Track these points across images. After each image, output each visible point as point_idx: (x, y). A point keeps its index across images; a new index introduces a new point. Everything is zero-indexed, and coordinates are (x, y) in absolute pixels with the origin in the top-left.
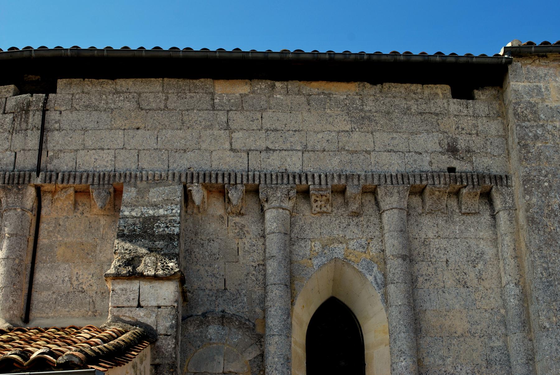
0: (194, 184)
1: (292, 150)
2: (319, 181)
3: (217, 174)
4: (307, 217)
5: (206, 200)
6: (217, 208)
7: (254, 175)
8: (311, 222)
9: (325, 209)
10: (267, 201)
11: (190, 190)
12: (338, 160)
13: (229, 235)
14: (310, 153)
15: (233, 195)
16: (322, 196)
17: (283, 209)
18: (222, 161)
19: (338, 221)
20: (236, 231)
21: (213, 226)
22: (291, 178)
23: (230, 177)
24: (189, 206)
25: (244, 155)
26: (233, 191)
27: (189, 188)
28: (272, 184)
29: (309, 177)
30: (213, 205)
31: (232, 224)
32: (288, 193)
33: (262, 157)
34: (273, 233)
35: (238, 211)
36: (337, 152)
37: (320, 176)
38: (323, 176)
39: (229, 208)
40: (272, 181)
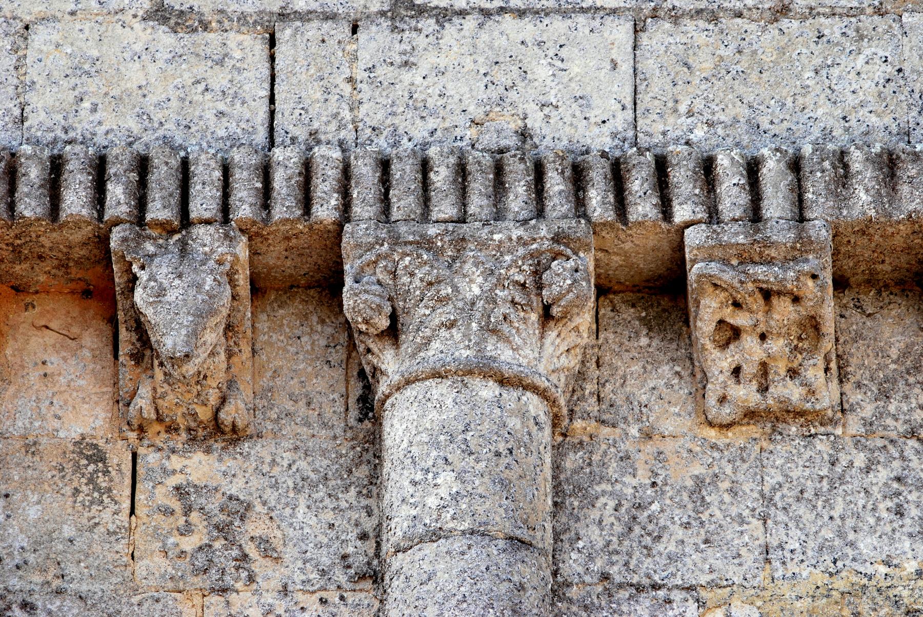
1: (566, 14)
2: (744, 199)
3: (56, 166)
4: (669, 446)
7: (307, 169)
8: (699, 482)
9: (793, 392)
10: (393, 333)
12: (880, 71)
13: (141, 568)
14: (689, 25)
15: (161, 292)
16: (767, 295)
17: (503, 381)
18: (92, 85)
19: (883, 475)
20: (189, 543)
21: (33, 513)
22: (556, 184)
25: (248, 47)
26: (163, 269)
28: (425, 217)
29: (682, 178)
30: (34, 376)
31: (163, 496)
32: (537, 274)
33: (365, 58)
34: (435, 535)
35: (204, 414)
36: (867, 22)
37: (753, 168)
38: (773, 170)
39: (145, 391)
40: (426, 201)
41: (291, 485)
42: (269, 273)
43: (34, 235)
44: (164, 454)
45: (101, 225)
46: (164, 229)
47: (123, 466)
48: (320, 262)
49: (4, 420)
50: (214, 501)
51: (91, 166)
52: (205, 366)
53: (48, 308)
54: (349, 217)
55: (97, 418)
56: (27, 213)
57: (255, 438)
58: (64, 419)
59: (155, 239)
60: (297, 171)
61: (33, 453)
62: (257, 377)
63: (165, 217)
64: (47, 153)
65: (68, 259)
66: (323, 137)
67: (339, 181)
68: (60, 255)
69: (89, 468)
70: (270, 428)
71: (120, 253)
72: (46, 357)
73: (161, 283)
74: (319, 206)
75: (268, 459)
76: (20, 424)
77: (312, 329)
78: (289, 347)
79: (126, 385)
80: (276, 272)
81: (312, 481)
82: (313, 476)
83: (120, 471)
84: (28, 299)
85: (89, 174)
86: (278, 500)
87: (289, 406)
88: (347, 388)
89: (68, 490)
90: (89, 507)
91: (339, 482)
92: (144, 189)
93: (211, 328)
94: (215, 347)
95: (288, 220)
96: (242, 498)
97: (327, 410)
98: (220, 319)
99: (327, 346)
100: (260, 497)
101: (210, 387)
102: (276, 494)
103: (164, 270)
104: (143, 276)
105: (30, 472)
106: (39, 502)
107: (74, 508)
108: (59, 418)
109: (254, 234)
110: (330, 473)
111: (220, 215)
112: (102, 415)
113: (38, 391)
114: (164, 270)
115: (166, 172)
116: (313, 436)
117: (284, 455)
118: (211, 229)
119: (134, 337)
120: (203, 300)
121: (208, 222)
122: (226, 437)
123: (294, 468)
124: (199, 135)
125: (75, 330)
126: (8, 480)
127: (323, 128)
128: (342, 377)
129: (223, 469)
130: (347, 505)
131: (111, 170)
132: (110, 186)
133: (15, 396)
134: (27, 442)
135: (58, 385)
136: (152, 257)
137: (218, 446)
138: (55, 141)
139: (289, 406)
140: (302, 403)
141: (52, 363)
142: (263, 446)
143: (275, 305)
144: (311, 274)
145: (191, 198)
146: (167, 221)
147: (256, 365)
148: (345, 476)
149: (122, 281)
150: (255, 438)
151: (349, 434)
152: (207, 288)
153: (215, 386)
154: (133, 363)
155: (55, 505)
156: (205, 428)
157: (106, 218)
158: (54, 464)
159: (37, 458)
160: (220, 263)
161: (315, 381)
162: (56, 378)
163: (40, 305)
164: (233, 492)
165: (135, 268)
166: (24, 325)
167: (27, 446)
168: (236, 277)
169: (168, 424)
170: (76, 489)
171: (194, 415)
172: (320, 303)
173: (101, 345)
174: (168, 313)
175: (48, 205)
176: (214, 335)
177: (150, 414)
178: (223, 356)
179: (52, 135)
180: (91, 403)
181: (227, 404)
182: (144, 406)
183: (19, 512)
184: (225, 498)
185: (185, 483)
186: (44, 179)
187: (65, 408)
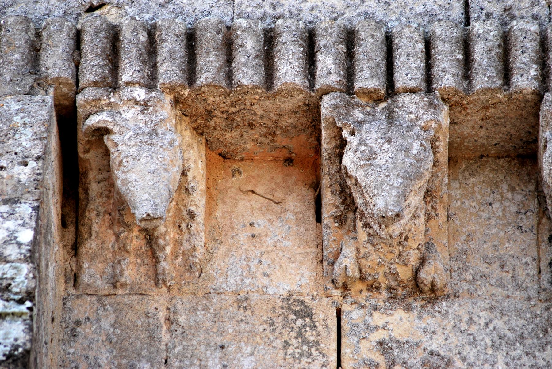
0: (126, 93)
3: (269, 39)
5: (198, 202)
6: (265, 249)
7: (506, 43)
11: (102, 132)
15: (372, 156)
23: (350, 55)
24: (91, 246)
26: (372, 134)
27: (94, 120)
30: (243, 237)
35: (405, 274)
39: (349, 251)
41: (489, 343)
42: (462, 142)
43: (248, 103)
44: (367, 311)
45: (312, 94)
46: (371, 98)
47: (329, 322)
48: (513, 132)
49: (217, 277)
50: (415, 356)
51: (302, 38)
52: (407, 228)
53: (253, 174)
54: (547, 87)
55: (302, 276)
56: (245, 82)
57: (452, 298)
58: (272, 277)
59: (363, 107)
60: (497, 43)
61: (245, 308)
62: (451, 241)
63: (373, 86)
64: (260, 26)
65: (277, 127)
66: (517, 13)
67: (537, 53)
68: (269, 123)
69: (297, 323)
70: (466, 288)
71: (331, 120)
72: (253, 220)
73: (371, 147)
74: (518, 76)
75: (466, 318)
76: (232, 281)
77: (502, 197)
78: (481, 213)
79: (330, 246)
80: (469, 142)
81: (509, 339)
82: (509, 334)
83: (326, 326)
84: (235, 166)
85: (301, 45)
86: (477, 357)
87: (483, 268)
88: (539, 254)
89: (279, 343)
90: (299, 359)
91: (535, 341)
92: (351, 60)
95: (489, 89)
96: (442, 354)
97: (521, 272)
98: (422, 184)
99: (518, 213)
100: (460, 353)
102: (475, 350)
103: (374, 135)
104: (353, 141)
105: (243, 325)
106: (252, 354)
107: (285, 359)
108: (268, 276)
109: (454, 103)
110: (526, 332)
111: (423, 86)
112: (308, 274)
113: (247, 250)
115: (372, 44)
116: (508, 297)
117: (481, 314)
118: (416, 98)
120: (411, 164)
121: (413, 91)
122: (425, 296)
123: (491, 327)
124: (398, 11)
125: (279, 195)
126: (222, 332)
127: (517, 4)
128: (534, 242)
129: (423, 326)
130: (545, 363)
131: (321, 42)
132: (320, 57)
133: (226, 255)
134: (239, 297)
135: (265, 246)
136: (361, 123)
137: (417, 304)
138: (263, 17)
139: (483, 268)
140: (496, 266)
141: (259, 225)
142: (460, 305)
143: (466, 173)
144: (502, 144)
145: (396, 69)
146: (375, 90)
147: (451, 229)
148: (541, 336)
149: (330, 146)
150: (452, 298)
151: (543, 296)
152: (415, 152)
153: (415, 247)
154: (337, 225)
155: (267, 356)
156: (404, 287)
157: (317, 86)
158: (265, 318)
159: (249, 313)
160: (425, 129)
161: (507, 245)
162: (263, 239)
163: (246, 171)
164: (434, 347)
165: (345, 134)
166: (232, 190)
167: (239, 301)
168: (437, 143)
169: (370, 283)
170: (286, 342)
171: (395, 275)
172: (510, 172)
173: (304, 209)
174: (379, 175)
175: (264, 74)
176: (417, 198)
177: (354, 272)
178: (422, 220)
179: (262, 10)
180: (297, 262)
181: (427, 264)
182: (348, 265)
183: (235, 362)
184: (426, 354)
185: (387, 338)
186: (259, 50)
187: (273, 266)
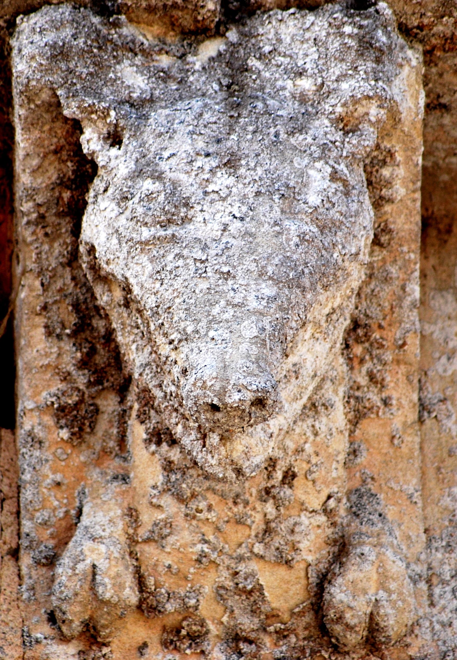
15: (176, 211)
39: (103, 518)
46: (172, 24)
52: (291, 445)
59: (147, 54)
62: (432, 484)
71: (45, 96)
73: (175, 184)
93: (317, 325)
94: (319, 388)
98: (337, 300)
101: (302, 507)
104: (117, 163)
114: (183, 145)
119: (70, 355)
120: (302, 237)
136: (141, 106)
147: (430, 448)
149: (41, 181)
154: (65, 434)
165: (91, 140)
168: (386, 172)
169: (170, 621)
171: (252, 594)
176: (322, 348)
177: (121, 587)
178: (339, 417)
182: (102, 564)
